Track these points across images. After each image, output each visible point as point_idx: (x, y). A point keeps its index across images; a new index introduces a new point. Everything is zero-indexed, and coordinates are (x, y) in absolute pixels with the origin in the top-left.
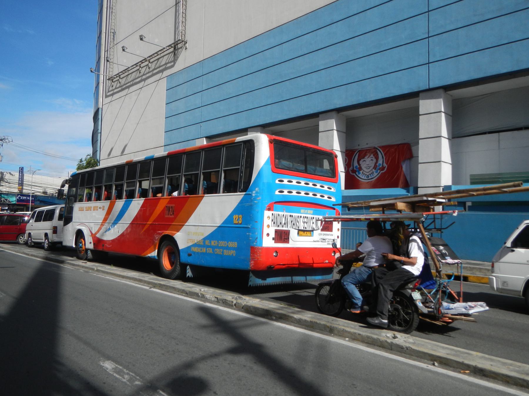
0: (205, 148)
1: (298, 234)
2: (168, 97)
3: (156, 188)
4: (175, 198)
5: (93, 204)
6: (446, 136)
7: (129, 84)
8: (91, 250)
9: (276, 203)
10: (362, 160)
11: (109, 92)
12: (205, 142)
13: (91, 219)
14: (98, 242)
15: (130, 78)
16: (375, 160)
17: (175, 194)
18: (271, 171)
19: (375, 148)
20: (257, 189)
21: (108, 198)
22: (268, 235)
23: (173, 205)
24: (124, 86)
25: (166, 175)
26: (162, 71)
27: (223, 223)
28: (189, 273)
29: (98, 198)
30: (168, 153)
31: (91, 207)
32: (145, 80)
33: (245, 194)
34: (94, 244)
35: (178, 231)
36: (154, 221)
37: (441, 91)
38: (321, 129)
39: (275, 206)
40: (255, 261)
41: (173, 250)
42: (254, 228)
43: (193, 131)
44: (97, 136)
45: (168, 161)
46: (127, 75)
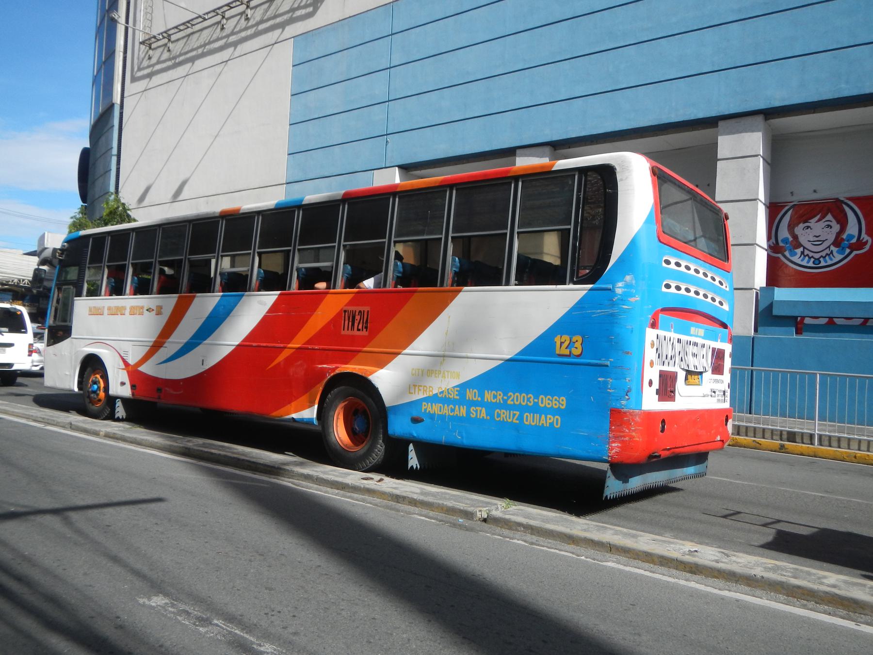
1: (686, 379)
2: (295, 79)
4: (368, 292)
6: (763, 201)
7: (194, 53)
8: (125, 400)
9: (665, 310)
10: (802, 226)
11: (139, 69)
12: (395, 178)
15: (194, 42)
16: (836, 227)
17: (369, 283)
19: (837, 200)
20: (628, 278)
22: (651, 383)
23: (366, 309)
24: (181, 58)
26: (282, 26)
27: (522, 352)
28: (413, 461)
31: (124, 308)
32: (235, 44)
33: (591, 290)
34: (133, 387)
35: (381, 365)
36: (309, 342)
37: (760, 119)
39: (662, 317)
40: (623, 442)
43: (366, 153)
44: (110, 161)
45: (344, 212)
46: (189, 35)
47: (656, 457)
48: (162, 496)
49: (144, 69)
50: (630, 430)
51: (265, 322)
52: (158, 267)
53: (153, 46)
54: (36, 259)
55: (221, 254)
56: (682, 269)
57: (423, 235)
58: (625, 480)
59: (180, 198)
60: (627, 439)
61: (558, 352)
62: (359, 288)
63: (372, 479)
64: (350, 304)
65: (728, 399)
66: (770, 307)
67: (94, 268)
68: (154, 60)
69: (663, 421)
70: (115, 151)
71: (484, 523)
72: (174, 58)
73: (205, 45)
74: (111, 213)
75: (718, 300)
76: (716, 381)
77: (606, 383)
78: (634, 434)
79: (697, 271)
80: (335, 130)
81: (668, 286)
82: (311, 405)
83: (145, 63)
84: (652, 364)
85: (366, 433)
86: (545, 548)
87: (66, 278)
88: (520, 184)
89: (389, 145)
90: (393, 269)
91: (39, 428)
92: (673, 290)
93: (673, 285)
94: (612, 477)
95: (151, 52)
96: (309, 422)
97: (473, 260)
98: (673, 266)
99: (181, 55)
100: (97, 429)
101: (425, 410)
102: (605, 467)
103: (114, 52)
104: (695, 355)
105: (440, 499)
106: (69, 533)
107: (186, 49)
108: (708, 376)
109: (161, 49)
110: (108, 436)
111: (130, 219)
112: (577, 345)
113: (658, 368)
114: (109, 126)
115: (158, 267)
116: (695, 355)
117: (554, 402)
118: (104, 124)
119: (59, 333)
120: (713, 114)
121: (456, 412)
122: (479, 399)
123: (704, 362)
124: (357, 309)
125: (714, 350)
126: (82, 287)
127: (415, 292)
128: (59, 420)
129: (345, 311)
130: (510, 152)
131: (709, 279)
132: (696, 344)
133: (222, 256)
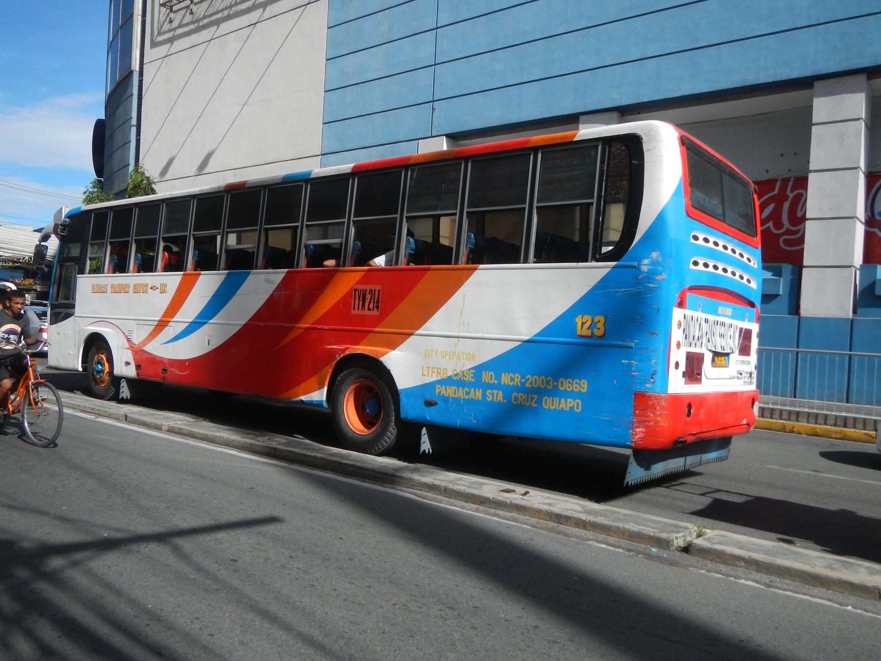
0: (363, 172)
1: (713, 360)
2: (330, 41)
3: (315, 246)
4: (379, 270)
5: (132, 278)
7: (219, 15)
8: (129, 381)
9: (693, 289)
11: (160, 34)
12: (443, 145)
13: (141, 314)
14: (142, 359)
17: (380, 261)
18: (684, 213)
20: (654, 255)
21: (174, 264)
22: (677, 365)
23: (377, 287)
24: (206, 21)
25: (108, 239)
27: (538, 334)
28: (426, 445)
29: (146, 266)
30: (355, 167)
31: (128, 286)
33: (615, 267)
34: (138, 367)
35: (393, 346)
36: (318, 322)
37: (863, 78)
38: (817, 117)
39: (690, 296)
41: (376, 386)
42: (647, 349)
43: (410, 122)
45: (354, 186)
47: (681, 442)
48: (275, 513)
49: (165, 33)
50: (654, 414)
51: (271, 304)
52: (162, 244)
53: (175, 8)
54: (38, 235)
55: (226, 230)
56: (711, 245)
57: (437, 210)
58: (648, 468)
59: (206, 170)
60: (652, 423)
61: (579, 333)
62: (370, 265)
63: (514, 491)
64: (361, 282)
65: (754, 380)
66: (873, 285)
67: (97, 244)
68: (175, 24)
69: (690, 405)
70: (134, 121)
71: (685, 555)
72: (198, 21)
73: (231, 7)
74: (135, 187)
75: (745, 278)
76: (743, 362)
77: (630, 365)
78: (659, 419)
79: (725, 248)
80: (375, 97)
81: (696, 263)
82: (321, 387)
83: (166, 27)
84: (678, 345)
85: (377, 417)
86: (789, 593)
87: (68, 253)
88: (540, 155)
89: (435, 113)
90: (405, 245)
91: (90, 420)
92: (700, 267)
93: (701, 262)
94: (635, 463)
95: (172, 15)
96: (319, 404)
97: (488, 234)
98: (700, 242)
99: (204, 17)
100: (159, 422)
101: (439, 393)
102: (629, 452)
103: (132, 16)
104: (722, 336)
105: (615, 521)
106: (182, 566)
107: (211, 11)
108: (735, 357)
109: (183, 12)
110: (171, 431)
111: (153, 192)
112: (598, 325)
113: (684, 350)
114: (127, 95)
115: (162, 244)
116: (722, 336)
117: (575, 385)
118: (122, 92)
119: (63, 310)
120: (809, 73)
121: (472, 395)
122: (496, 382)
123: (732, 343)
124: (368, 287)
125: (741, 329)
126: (85, 263)
127: (428, 269)
128: (112, 411)
129: (355, 290)
130: (573, 119)
131: (737, 256)
132: (723, 324)
133: (228, 233)
